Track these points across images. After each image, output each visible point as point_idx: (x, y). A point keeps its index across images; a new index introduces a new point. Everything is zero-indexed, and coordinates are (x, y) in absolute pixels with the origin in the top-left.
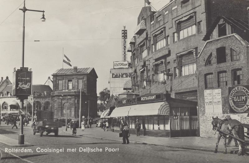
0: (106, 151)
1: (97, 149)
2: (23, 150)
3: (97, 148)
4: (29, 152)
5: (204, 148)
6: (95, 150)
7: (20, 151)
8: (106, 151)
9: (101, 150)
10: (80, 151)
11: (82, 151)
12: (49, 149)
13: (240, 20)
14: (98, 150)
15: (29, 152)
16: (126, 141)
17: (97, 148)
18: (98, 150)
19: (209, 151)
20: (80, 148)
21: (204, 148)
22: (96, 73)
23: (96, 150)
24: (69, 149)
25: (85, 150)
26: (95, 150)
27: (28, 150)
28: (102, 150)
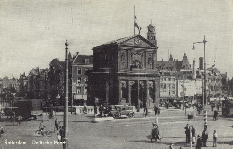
0: (55, 144)
1: (47, 142)
2: (19, 142)
3: (47, 141)
4: (25, 144)
5: (167, 97)
6: (46, 143)
7: (17, 143)
8: (55, 144)
9: (51, 143)
10: (33, 144)
11: (34, 144)
12: (20, 142)
13: (143, 104)
14: (48, 143)
15: (25, 144)
16: (54, 72)
17: (47, 141)
18: (48, 143)
19: (130, 39)
20: (33, 141)
21: (167, 97)
22: (200, 64)
23: (47, 143)
24: (25, 143)
25: (37, 143)
26: (46, 143)
27: (23, 143)
28: (51, 143)
